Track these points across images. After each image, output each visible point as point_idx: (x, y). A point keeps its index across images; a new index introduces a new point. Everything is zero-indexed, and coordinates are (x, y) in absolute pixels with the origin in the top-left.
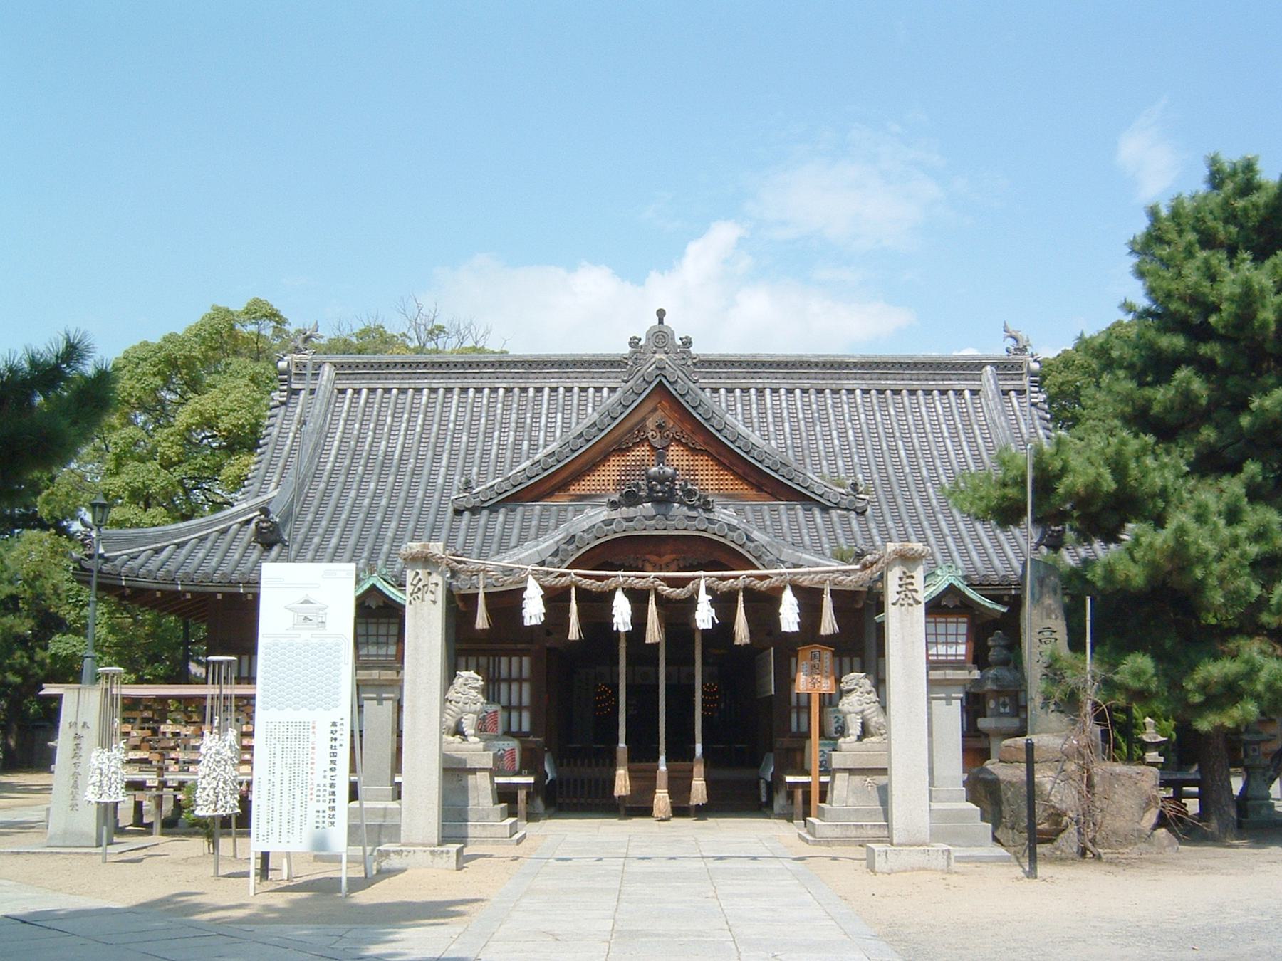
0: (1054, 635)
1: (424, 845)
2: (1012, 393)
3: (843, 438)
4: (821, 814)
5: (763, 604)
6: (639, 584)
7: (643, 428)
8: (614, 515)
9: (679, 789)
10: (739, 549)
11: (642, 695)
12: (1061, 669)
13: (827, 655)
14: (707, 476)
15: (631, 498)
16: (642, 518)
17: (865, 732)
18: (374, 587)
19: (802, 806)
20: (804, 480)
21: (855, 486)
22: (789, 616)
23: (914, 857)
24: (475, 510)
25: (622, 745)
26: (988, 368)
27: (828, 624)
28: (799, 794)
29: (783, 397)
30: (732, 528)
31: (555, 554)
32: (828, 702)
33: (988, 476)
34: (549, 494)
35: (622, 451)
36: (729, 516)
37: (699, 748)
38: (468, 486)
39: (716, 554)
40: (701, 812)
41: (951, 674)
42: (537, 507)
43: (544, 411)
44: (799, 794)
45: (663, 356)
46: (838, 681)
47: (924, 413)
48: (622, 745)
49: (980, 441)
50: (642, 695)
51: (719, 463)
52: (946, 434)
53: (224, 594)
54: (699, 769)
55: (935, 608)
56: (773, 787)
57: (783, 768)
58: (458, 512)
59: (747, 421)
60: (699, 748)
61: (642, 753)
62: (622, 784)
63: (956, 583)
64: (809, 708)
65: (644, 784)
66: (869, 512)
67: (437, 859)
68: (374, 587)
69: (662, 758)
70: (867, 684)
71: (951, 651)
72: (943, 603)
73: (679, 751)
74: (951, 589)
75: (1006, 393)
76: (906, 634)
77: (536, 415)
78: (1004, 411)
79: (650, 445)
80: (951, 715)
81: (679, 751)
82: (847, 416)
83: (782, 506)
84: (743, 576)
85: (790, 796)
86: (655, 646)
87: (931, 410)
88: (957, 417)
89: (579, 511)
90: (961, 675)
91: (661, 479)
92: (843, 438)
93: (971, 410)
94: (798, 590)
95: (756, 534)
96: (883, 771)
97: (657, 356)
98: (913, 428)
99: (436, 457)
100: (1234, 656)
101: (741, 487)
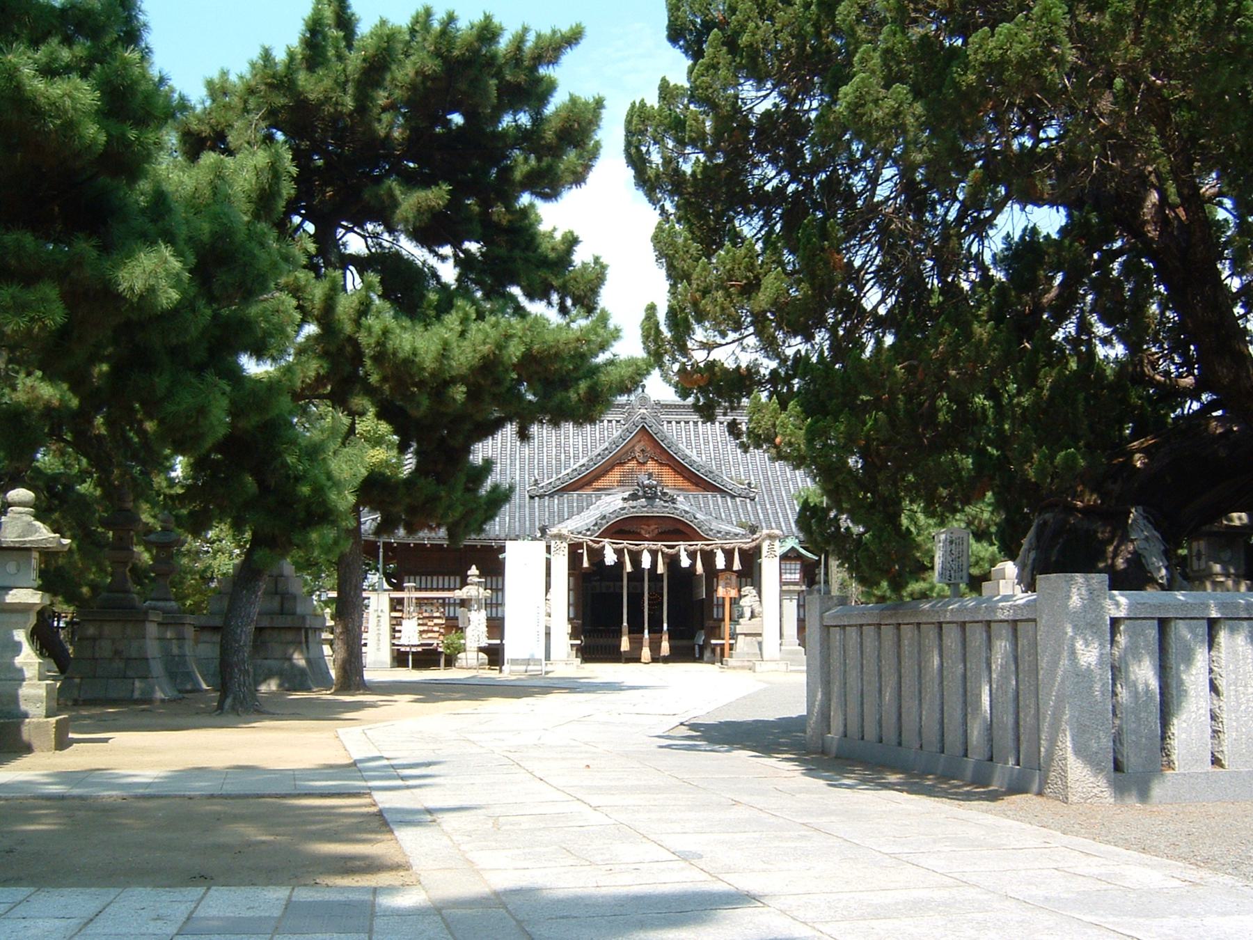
4: (731, 656)
5: (708, 557)
6: (654, 547)
7: (633, 451)
9: (655, 647)
11: (636, 600)
13: (734, 577)
14: (669, 479)
15: (634, 497)
16: (640, 507)
17: (753, 616)
19: (718, 656)
21: (749, 484)
22: (720, 562)
23: (772, 666)
24: (541, 497)
25: (625, 624)
27: (737, 565)
28: (718, 649)
30: (687, 512)
31: (596, 525)
32: (734, 602)
34: (581, 488)
35: (621, 464)
36: (686, 504)
37: (665, 626)
38: (536, 483)
39: (678, 530)
40: (666, 660)
41: (792, 588)
42: (575, 494)
44: (718, 649)
46: (739, 591)
48: (625, 624)
50: (636, 600)
51: (675, 471)
54: (665, 637)
55: (785, 557)
56: (702, 648)
57: (709, 637)
58: (532, 497)
59: (689, 442)
60: (665, 626)
61: (636, 629)
62: (625, 645)
64: (723, 605)
65: (637, 645)
69: (646, 631)
70: (754, 592)
73: (656, 628)
76: (770, 568)
80: (791, 607)
81: (656, 628)
83: (709, 495)
84: (700, 544)
85: (713, 651)
86: (701, 576)
89: (598, 498)
90: (797, 588)
91: (650, 487)
94: (724, 550)
95: (698, 516)
96: (760, 635)
99: (512, 463)
100: (924, 580)
101: (687, 484)
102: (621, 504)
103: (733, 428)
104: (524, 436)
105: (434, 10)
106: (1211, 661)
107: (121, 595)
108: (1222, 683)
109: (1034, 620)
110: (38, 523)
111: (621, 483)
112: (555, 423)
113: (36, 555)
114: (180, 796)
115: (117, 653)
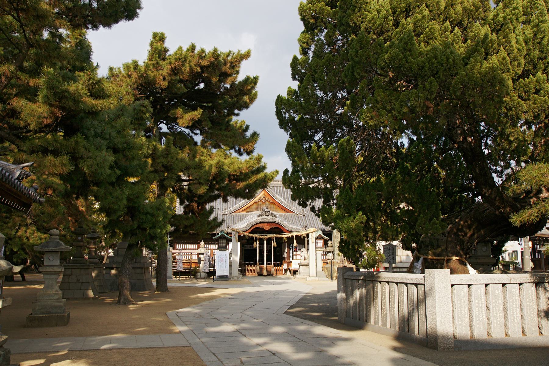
14: (274, 209)
55: (317, 238)
74: (320, 235)
102: (256, 218)
103: (313, 209)
104: (225, 201)
105: (250, 128)
106: (486, 298)
107: (80, 259)
108: (491, 307)
109: (424, 285)
110: (61, 242)
111: (257, 210)
112: (95, 27)
113: (60, 253)
114: (129, 349)
115: (78, 280)
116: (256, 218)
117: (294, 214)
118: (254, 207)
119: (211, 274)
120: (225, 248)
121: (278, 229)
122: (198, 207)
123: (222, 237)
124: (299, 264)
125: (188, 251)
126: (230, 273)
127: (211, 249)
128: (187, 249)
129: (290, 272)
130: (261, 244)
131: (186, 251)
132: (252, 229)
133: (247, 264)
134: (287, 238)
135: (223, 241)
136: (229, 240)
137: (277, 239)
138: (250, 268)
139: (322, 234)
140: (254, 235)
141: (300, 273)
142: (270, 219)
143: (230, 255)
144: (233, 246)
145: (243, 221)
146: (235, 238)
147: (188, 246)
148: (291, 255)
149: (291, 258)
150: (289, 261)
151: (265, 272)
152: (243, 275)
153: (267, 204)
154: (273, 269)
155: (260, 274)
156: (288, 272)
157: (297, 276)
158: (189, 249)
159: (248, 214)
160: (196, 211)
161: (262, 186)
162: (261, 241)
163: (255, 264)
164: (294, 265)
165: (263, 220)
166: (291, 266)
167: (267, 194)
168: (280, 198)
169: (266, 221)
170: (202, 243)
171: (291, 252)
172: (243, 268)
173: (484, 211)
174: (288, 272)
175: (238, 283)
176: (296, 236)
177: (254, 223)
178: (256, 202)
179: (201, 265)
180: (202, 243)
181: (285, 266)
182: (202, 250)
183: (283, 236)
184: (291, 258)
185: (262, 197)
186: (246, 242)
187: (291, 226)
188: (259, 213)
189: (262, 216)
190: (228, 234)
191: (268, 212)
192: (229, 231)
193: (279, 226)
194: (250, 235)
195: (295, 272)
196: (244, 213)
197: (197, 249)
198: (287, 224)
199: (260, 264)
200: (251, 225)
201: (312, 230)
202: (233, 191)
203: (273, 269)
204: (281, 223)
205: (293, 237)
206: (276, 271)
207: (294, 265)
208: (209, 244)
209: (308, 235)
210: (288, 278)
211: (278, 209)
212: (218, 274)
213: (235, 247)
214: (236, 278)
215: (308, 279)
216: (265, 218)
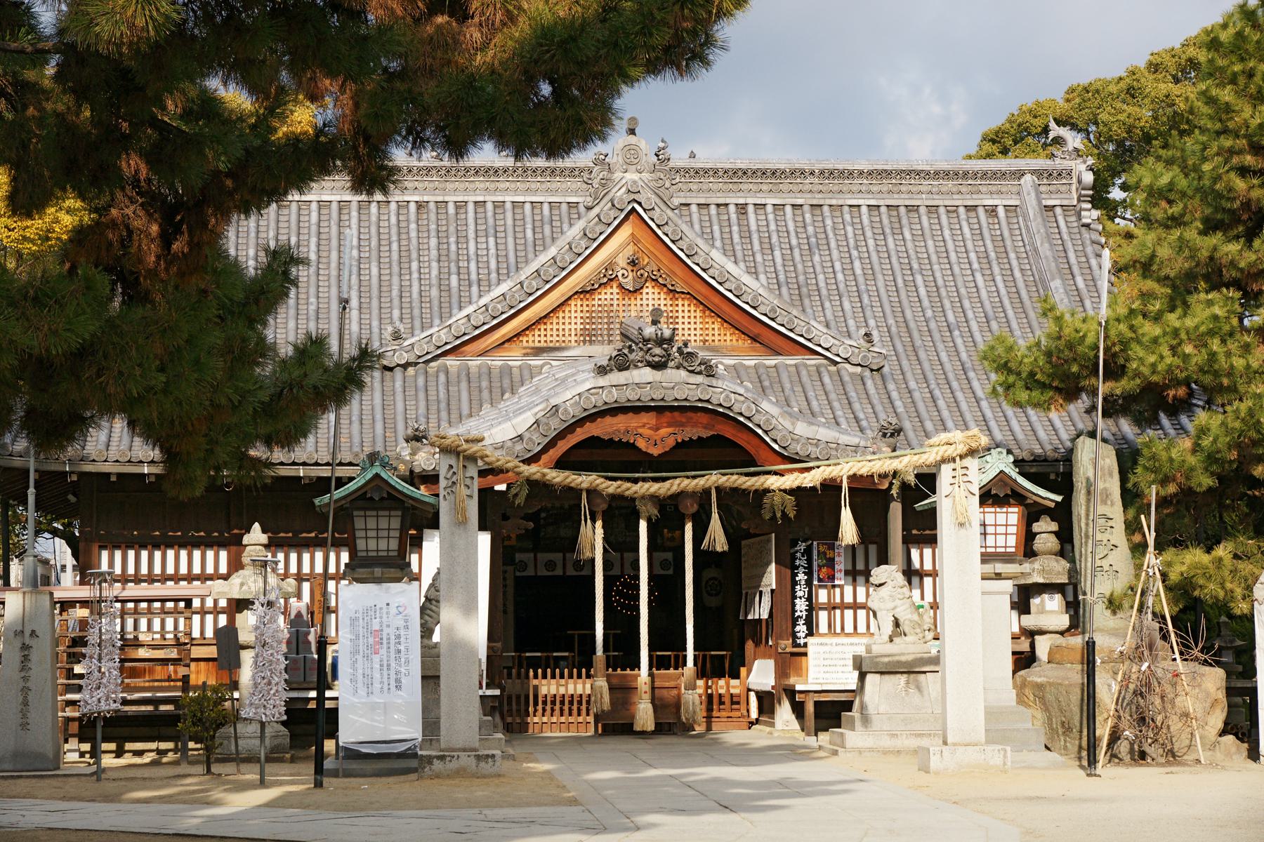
0: (1110, 523)
1: (464, 750)
2: (1058, 210)
3: (849, 270)
8: (602, 381)
10: (727, 412)
12: (1049, 409)
14: (691, 326)
18: (377, 476)
20: (808, 331)
26: (1028, 177)
29: (771, 217)
33: (1038, 344)
41: (1000, 568)
43: (471, 235)
45: (635, 176)
47: (948, 237)
49: (1017, 274)
52: (976, 266)
53: (119, 475)
55: (989, 497)
63: (1007, 470)
66: (886, 370)
67: (482, 764)
68: (377, 476)
71: (383, 545)
72: (993, 492)
74: (1002, 477)
75: (1051, 208)
77: (461, 238)
78: (1048, 235)
79: (621, 286)
82: (852, 242)
87: (957, 232)
88: (989, 243)
92: (849, 270)
93: (1006, 234)
97: (628, 176)
98: (934, 258)
102: (588, 381)
111: (588, 336)
116: (588, 381)
117: (813, 361)
118: (574, 317)
119: (309, 724)
120: (394, 567)
121: (723, 441)
122: (166, 239)
123: (378, 497)
124: (858, 663)
125: (170, 589)
126: (431, 725)
127: (311, 577)
128: (164, 578)
129: (798, 709)
130: (620, 544)
131: (157, 590)
132: (563, 446)
133: (535, 664)
134: (797, 492)
135: (378, 520)
136: (421, 520)
137: (729, 497)
138: (549, 687)
139: (1013, 473)
140: (584, 480)
141: (866, 720)
142: (675, 383)
143: (429, 609)
144: (447, 552)
145: (509, 403)
146: (459, 499)
147: (172, 560)
148: (801, 605)
149: (801, 629)
150: (786, 645)
151: (644, 715)
152: (508, 729)
153: (652, 297)
154: (690, 688)
155: (616, 725)
156: (784, 712)
157: (853, 736)
158: (176, 578)
159: (536, 362)
160: (152, 274)
161: (661, 38)
162: (620, 516)
163: (583, 664)
164: (826, 666)
165: (632, 395)
166: (800, 672)
167: (647, 241)
168: (730, 267)
169: (646, 396)
170: (256, 536)
171: (801, 591)
172: (513, 686)
173: (809, 573)
174: (784, 712)
175: (480, 791)
176: (853, 478)
177: (574, 412)
178: (584, 292)
179: (246, 674)
180: (256, 536)
181: (761, 674)
182: (246, 583)
183: (773, 482)
184: (801, 629)
185: (622, 261)
186: (528, 525)
187: (802, 429)
188: (602, 353)
189: (623, 368)
190: (414, 478)
191: (660, 341)
192: (425, 459)
193: (728, 432)
194: (557, 477)
195: (830, 713)
196: (513, 358)
197: (225, 578)
198: (774, 417)
199: (611, 663)
200: (556, 425)
201: (958, 439)
202: (428, 89)
203: (693, 697)
204: (741, 407)
205: (831, 487)
206: (710, 701)
207: (826, 666)
208: (302, 545)
209: (928, 480)
210: (792, 752)
211: (717, 333)
212: (355, 728)
213: (459, 565)
214: (467, 761)
215: (935, 762)
216: (642, 381)
